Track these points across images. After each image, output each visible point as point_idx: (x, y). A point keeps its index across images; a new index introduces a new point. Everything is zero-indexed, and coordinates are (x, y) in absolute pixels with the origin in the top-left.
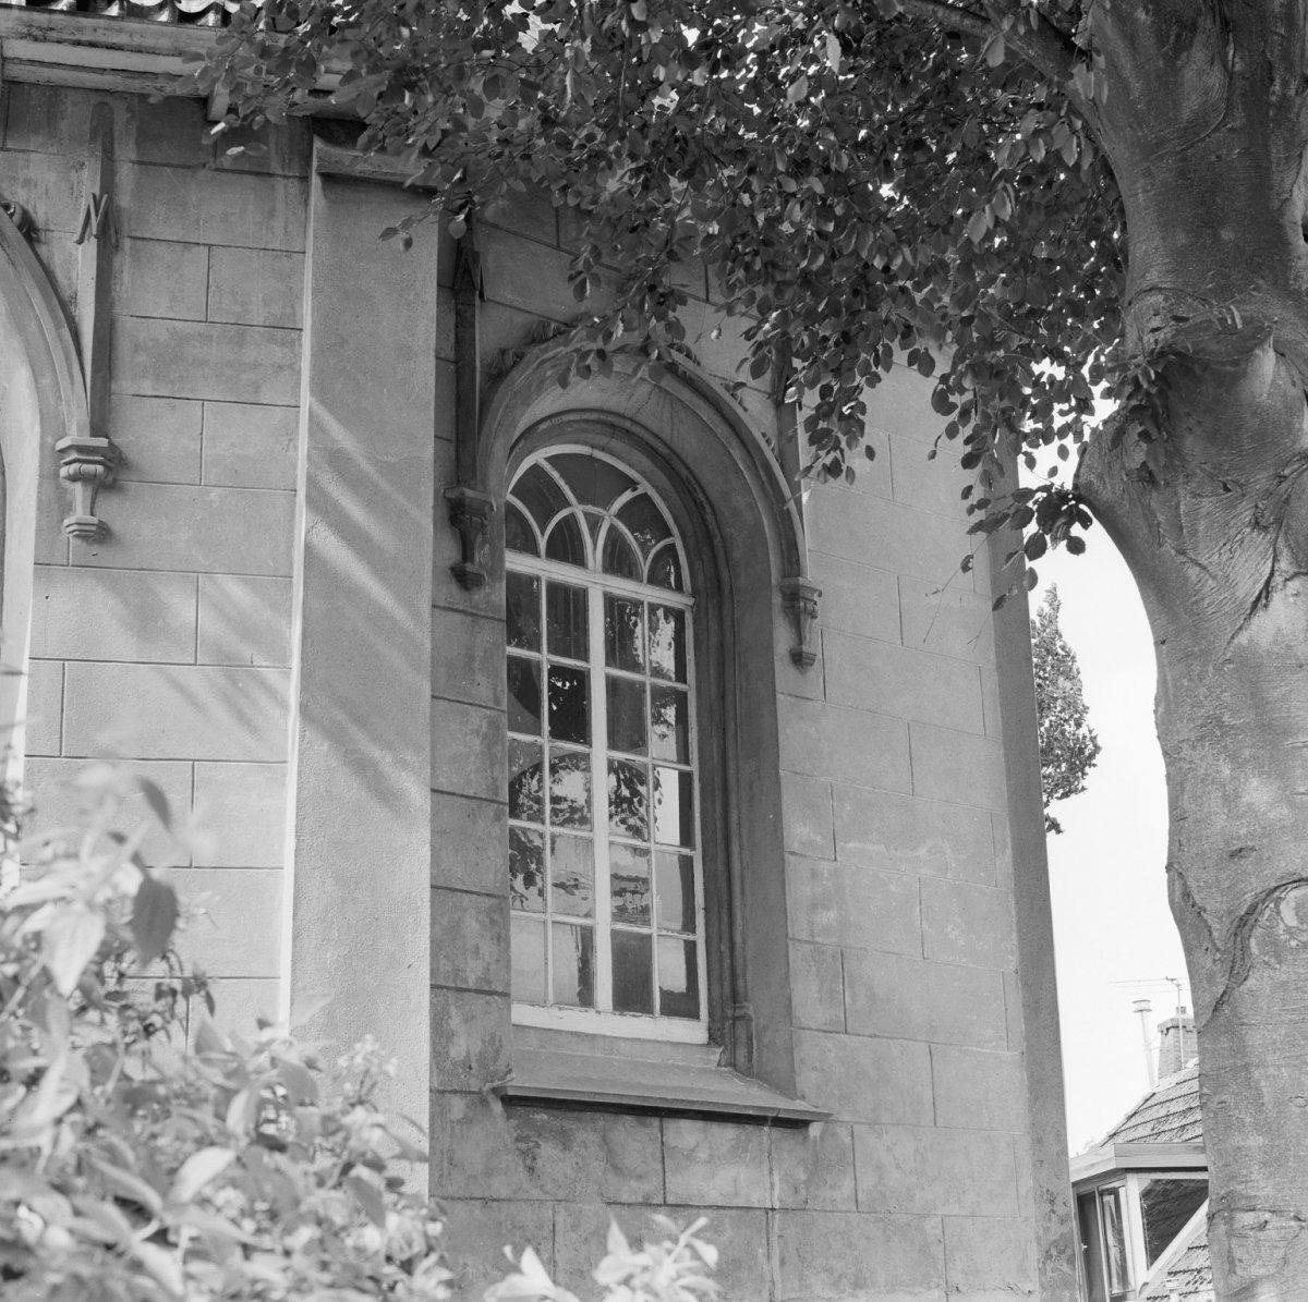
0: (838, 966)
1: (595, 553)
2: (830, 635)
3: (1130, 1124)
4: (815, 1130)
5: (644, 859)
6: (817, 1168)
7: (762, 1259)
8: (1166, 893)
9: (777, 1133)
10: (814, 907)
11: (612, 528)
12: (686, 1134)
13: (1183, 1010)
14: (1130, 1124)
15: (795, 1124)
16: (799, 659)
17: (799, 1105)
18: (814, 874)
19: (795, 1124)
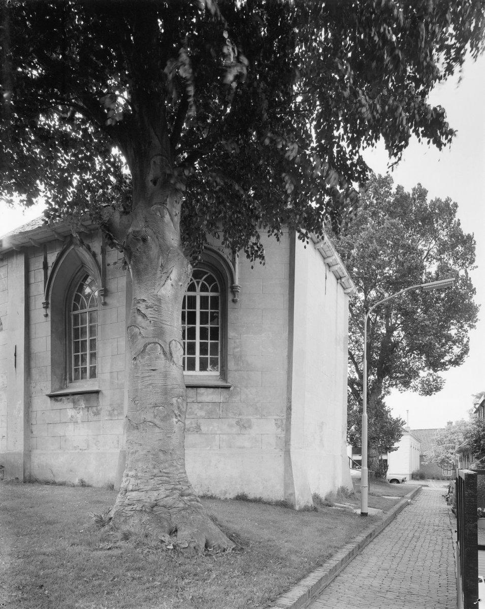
0: (239, 359)
1: (198, 288)
2: (241, 298)
3: (49, 272)
4: (231, 389)
5: (371, 492)
6: (231, 395)
7: (218, 411)
8: (294, 364)
9: (222, 389)
10: (234, 348)
11: (203, 283)
12: (202, 390)
13: (348, 390)
14: (49, 272)
15: (228, 388)
16: (234, 301)
17: (228, 384)
18: (235, 342)
19: (228, 388)
